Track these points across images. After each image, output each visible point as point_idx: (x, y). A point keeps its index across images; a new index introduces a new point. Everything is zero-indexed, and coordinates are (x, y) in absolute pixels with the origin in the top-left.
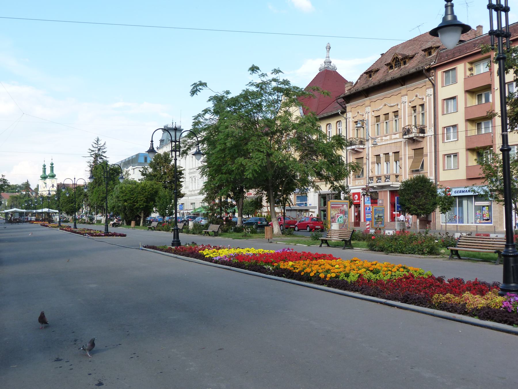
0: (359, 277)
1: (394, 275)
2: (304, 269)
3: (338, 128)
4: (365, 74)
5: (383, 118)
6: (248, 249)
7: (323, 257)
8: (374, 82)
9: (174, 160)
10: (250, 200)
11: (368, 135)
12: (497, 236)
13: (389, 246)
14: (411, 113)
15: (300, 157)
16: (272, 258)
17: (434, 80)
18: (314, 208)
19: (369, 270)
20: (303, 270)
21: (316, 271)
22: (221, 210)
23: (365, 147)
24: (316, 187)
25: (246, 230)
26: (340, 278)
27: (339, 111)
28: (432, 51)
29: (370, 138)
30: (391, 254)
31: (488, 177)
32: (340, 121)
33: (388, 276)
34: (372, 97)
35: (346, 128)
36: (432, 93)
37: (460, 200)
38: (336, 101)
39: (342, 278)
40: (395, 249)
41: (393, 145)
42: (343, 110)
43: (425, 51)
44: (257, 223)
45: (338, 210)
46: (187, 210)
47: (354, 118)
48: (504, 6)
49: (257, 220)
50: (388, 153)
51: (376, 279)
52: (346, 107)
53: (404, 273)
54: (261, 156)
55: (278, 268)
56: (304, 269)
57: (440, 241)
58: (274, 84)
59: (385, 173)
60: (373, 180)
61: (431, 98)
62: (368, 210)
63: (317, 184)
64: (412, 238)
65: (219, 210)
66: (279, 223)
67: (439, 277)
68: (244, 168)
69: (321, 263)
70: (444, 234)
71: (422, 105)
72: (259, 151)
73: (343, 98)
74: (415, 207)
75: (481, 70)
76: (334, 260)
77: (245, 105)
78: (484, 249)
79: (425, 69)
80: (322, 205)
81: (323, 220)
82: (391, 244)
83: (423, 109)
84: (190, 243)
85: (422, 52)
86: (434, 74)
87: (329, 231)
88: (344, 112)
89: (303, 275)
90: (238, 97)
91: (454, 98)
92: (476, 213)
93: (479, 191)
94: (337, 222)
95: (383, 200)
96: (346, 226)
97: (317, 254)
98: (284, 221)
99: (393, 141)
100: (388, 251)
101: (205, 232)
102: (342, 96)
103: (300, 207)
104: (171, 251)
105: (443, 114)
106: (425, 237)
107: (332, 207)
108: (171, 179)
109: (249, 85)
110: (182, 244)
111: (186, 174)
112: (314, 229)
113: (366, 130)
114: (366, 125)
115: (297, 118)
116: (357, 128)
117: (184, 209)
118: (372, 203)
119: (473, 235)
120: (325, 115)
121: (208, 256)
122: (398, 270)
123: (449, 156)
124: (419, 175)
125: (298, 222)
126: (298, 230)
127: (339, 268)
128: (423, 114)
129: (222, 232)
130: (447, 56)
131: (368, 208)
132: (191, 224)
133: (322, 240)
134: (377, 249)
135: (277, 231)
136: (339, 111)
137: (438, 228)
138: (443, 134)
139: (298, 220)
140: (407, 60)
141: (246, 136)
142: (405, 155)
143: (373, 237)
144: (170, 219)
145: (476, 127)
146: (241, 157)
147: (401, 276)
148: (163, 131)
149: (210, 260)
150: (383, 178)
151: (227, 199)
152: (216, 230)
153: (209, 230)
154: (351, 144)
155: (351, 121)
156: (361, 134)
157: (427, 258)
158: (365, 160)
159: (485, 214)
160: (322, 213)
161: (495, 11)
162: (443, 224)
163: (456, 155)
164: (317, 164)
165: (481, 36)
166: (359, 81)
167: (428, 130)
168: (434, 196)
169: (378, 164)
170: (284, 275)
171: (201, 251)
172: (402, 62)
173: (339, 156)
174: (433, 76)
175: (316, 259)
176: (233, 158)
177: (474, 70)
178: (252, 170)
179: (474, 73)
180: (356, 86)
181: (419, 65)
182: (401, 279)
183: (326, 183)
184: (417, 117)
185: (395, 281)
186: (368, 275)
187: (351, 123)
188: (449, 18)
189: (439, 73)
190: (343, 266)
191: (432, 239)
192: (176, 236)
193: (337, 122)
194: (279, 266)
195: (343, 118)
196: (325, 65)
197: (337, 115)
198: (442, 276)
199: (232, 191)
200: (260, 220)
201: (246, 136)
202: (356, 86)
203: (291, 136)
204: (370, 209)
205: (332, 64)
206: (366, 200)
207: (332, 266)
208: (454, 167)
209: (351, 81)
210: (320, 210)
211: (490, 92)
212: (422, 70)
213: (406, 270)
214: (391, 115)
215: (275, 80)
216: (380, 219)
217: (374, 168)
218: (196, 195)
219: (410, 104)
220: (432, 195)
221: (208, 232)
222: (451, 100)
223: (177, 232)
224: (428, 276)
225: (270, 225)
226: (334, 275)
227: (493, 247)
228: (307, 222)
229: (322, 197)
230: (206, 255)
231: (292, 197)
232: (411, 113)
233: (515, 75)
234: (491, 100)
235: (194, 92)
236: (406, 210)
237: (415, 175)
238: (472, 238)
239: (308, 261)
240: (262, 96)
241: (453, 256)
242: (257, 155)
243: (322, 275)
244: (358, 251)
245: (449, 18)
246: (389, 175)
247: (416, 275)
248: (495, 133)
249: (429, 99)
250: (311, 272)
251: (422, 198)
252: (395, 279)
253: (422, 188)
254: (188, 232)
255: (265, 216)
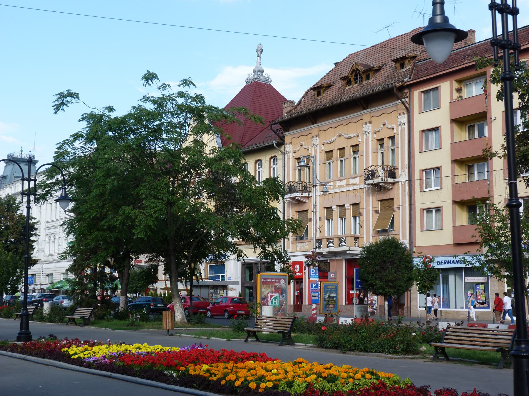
0: (307, 387)
1: (358, 384)
2: (226, 375)
3: (272, 166)
4: (312, 91)
5: (325, 156)
6: (138, 345)
7: (254, 357)
8: (324, 102)
9: (26, 207)
10: (138, 270)
11: (315, 179)
12: (498, 327)
13: (347, 341)
14: (377, 149)
15: (216, 208)
16: (176, 359)
17: (408, 102)
18: (236, 283)
19: (321, 377)
20: (224, 378)
21: (243, 379)
22: (96, 285)
23: (312, 194)
24: (239, 252)
25: (133, 316)
26: (280, 389)
27: (274, 142)
28: (407, 62)
29: (318, 182)
30: (350, 352)
31: (486, 242)
32: (276, 156)
33: (349, 386)
34: (321, 123)
35: (284, 167)
36: (406, 121)
37: (445, 274)
38: (269, 128)
39: (283, 388)
40: (355, 345)
41: (351, 193)
42: (280, 141)
43: (396, 62)
44: (149, 305)
45: (272, 287)
46: (40, 284)
47: (295, 153)
48: (511, 6)
49: (149, 301)
50: (344, 205)
51: (332, 390)
52: (284, 136)
53: (372, 381)
54: (159, 205)
55: (185, 374)
56: (226, 375)
57: (419, 333)
58: (180, 101)
59: (339, 233)
60: (321, 243)
61: (404, 128)
62: (315, 287)
63: (240, 248)
64: (379, 329)
65: (92, 285)
66: (184, 305)
67: (421, 387)
68: (133, 221)
69: (250, 366)
70: (424, 324)
71: (392, 138)
72: (156, 197)
73: (280, 123)
74: (382, 284)
75: (472, 92)
76: (270, 362)
77: (135, 129)
78: (481, 346)
79: (396, 87)
80: (248, 279)
81: (248, 302)
82: (349, 338)
83: (393, 143)
84: (47, 337)
85: (392, 62)
86: (408, 94)
87: (259, 318)
88: (281, 143)
89: (223, 385)
90: (126, 117)
91: (436, 129)
92: (467, 294)
93: (473, 262)
94: (270, 304)
95: (335, 273)
96: (284, 310)
97: (243, 353)
98: (191, 303)
99: (351, 188)
100: (346, 349)
101: (69, 318)
102: (279, 120)
103: (215, 282)
104: (15, 349)
105: (421, 152)
106: (397, 327)
107: (263, 283)
108: (16, 237)
109: (143, 100)
110: (34, 338)
111: (41, 229)
112: (236, 316)
113: (313, 171)
114: (313, 163)
115: (213, 150)
116: (299, 168)
117: (35, 283)
118: (320, 277)
119: (465, 326)
120: (254, 147)
121: (76, 357)
122: (363, 376)
123: (429, 211)
124: (387, 238)
125: (211, 305)
126: (212, 317)
127: (278, 374)
128: (393, 150)
129: (95, 319)
130: (427, 71)
131: (314, 285)
132: (46, 306)
133: (249, 332)
134: (329, 345)
135: (181, 318)
136: (274, 143)
137: (414, 314)
138: (421, 180)
139: (212, 301)
140: (371, 74)
141: (137, 174)
142: (368, 208)
143: (323, 328)
144: (12, 298)
145: (466, 171)
146: (128, 206)
147: (367, 385)
148: (6, 163)
149: (80, 362)
150: (336, 241)
151: (103, 268)
152: (87, 316)
153: (76, 317)
154: (291, 190)
155: (291, 157)
156: (306, 176)
157: (401, 358)
158: (310, 215)
159: (479, 295)
160: (247, 291)
161: (498, 13)
162: (421, 309)
163: (438, 210)
164: (241, 219)
165: (473, 44)
166: (303, 99)
167: (400, 173)
168: (409, 268)
169: (329, 220)
170: (194, 384)
171: (66, 349)
172: (364, 76)
173: (274, 209)
174: (407, 97)
175: (243, 360)
176: (116, 208)
177: (463, 91)
178: (145, 227)
179: (463, 96)
180: (299, 107)
181: (389, 80)
182: (368, 390)
183: (255, 247)
184: (385, 154)
185: (359, 393)
186: (320, 384)
187: (291, 159)
188: (439, 19)
189: (416, 94)
190: (284, 371)
191: (408, 330)
192: (24, 325)
193: (271, 158)
194: (188, 371)
195: (280, 153)
196: (255, 74)
197: (270, 148)
198: (426, 386)
199: (112, 256)
200: (154, 300)
201: (137, 174)
202: (298, 107)
203: (203, 177)
204: (317, 286)
205: (264, 74)
206: (311, 273)
207: (267, 371)
208: (436, 227)
209: (292, 100)
210: (244, 287)
211: (485, 122)
212: (392, 89)
213: (374, 377)
214: (349, 151)
215: (182, 95)
216: (331, 301)
217: (323, 226)
218: (55, 262)
219: (375, 136)
220: (406, 267)
221: (74, 319)
222: (431, 132)
223: (25, 319)
224: (406, 385)
225: (169, 308)
226: (270, 384)
227: (494, 343)
228: (225, 305)
229: (247, 268)
230: (73, 355)
231: (203, 267)
232: (377, 149)
233: (520, 100)
234: (486, 134)
235: (58, 107)
236: (369, 288)
237: (381, 238)
238: (464, 329)
239: (230, 364)
240: (162, 117)
241: (438, 355)
242: (153, 203)
243: (253, 385)
244: (301, 349)
245: (439, 19)
246: (344, 236)
247: (388, 383)
248: (492, 180)
249: (401, 130)
250: (236, 380)
251: (391, 271)
252: (359, 390)
253: (392, 256)
254: (42, 319)
255: (161, 295)
